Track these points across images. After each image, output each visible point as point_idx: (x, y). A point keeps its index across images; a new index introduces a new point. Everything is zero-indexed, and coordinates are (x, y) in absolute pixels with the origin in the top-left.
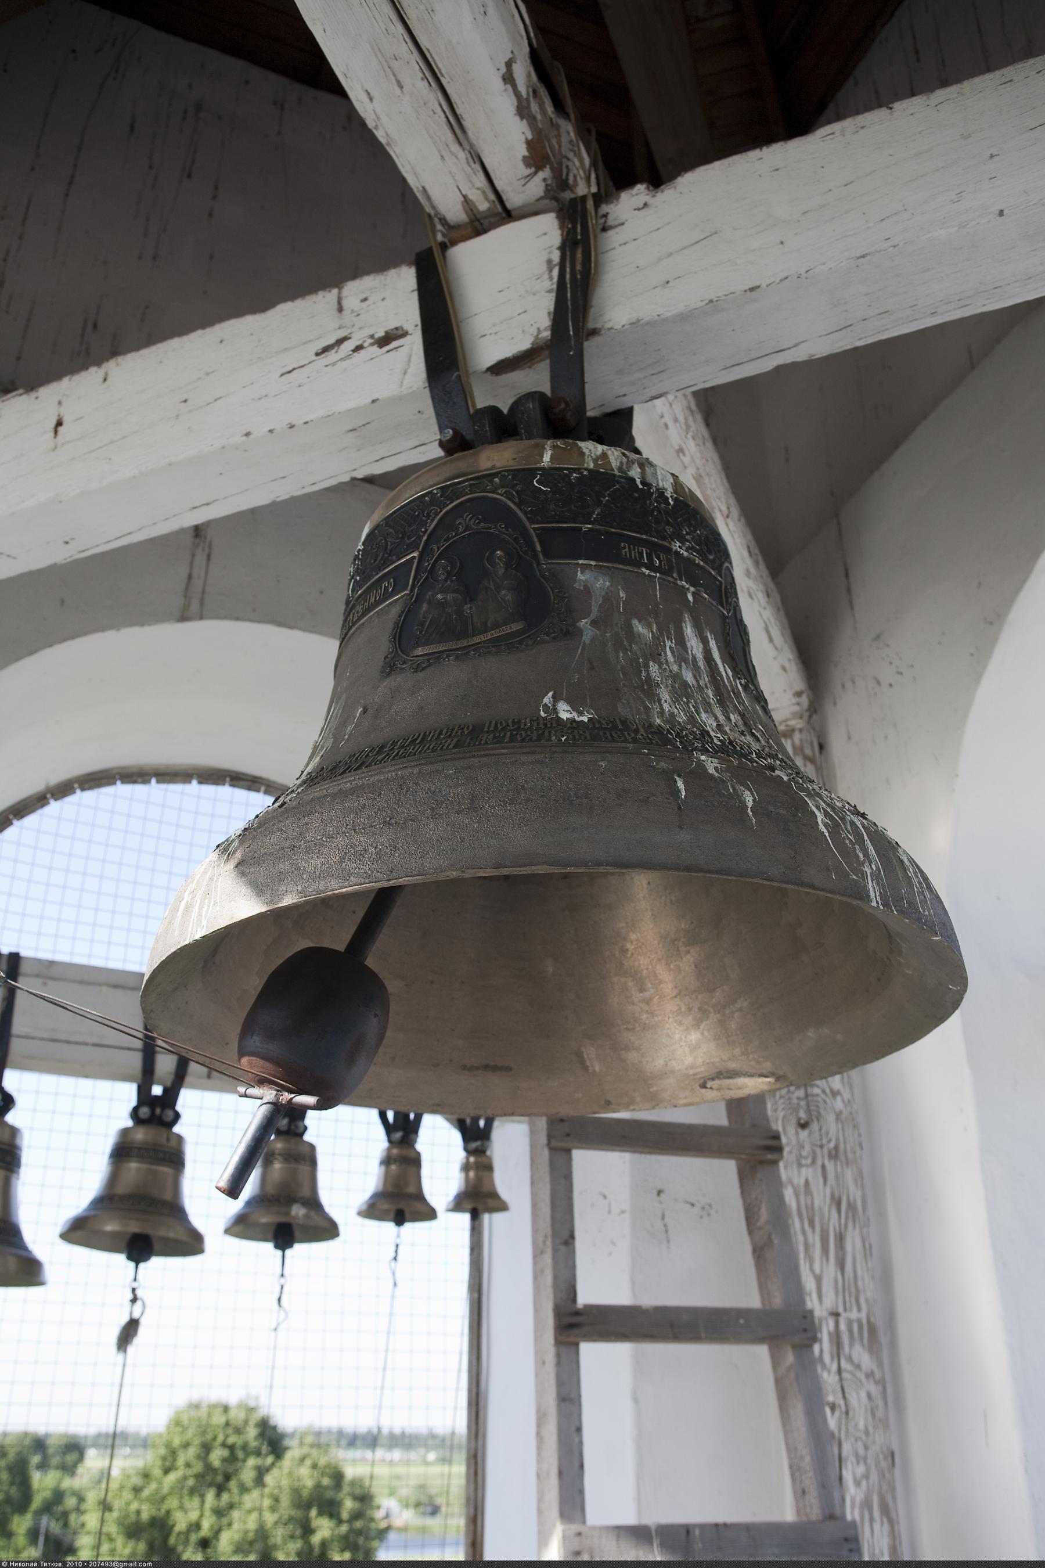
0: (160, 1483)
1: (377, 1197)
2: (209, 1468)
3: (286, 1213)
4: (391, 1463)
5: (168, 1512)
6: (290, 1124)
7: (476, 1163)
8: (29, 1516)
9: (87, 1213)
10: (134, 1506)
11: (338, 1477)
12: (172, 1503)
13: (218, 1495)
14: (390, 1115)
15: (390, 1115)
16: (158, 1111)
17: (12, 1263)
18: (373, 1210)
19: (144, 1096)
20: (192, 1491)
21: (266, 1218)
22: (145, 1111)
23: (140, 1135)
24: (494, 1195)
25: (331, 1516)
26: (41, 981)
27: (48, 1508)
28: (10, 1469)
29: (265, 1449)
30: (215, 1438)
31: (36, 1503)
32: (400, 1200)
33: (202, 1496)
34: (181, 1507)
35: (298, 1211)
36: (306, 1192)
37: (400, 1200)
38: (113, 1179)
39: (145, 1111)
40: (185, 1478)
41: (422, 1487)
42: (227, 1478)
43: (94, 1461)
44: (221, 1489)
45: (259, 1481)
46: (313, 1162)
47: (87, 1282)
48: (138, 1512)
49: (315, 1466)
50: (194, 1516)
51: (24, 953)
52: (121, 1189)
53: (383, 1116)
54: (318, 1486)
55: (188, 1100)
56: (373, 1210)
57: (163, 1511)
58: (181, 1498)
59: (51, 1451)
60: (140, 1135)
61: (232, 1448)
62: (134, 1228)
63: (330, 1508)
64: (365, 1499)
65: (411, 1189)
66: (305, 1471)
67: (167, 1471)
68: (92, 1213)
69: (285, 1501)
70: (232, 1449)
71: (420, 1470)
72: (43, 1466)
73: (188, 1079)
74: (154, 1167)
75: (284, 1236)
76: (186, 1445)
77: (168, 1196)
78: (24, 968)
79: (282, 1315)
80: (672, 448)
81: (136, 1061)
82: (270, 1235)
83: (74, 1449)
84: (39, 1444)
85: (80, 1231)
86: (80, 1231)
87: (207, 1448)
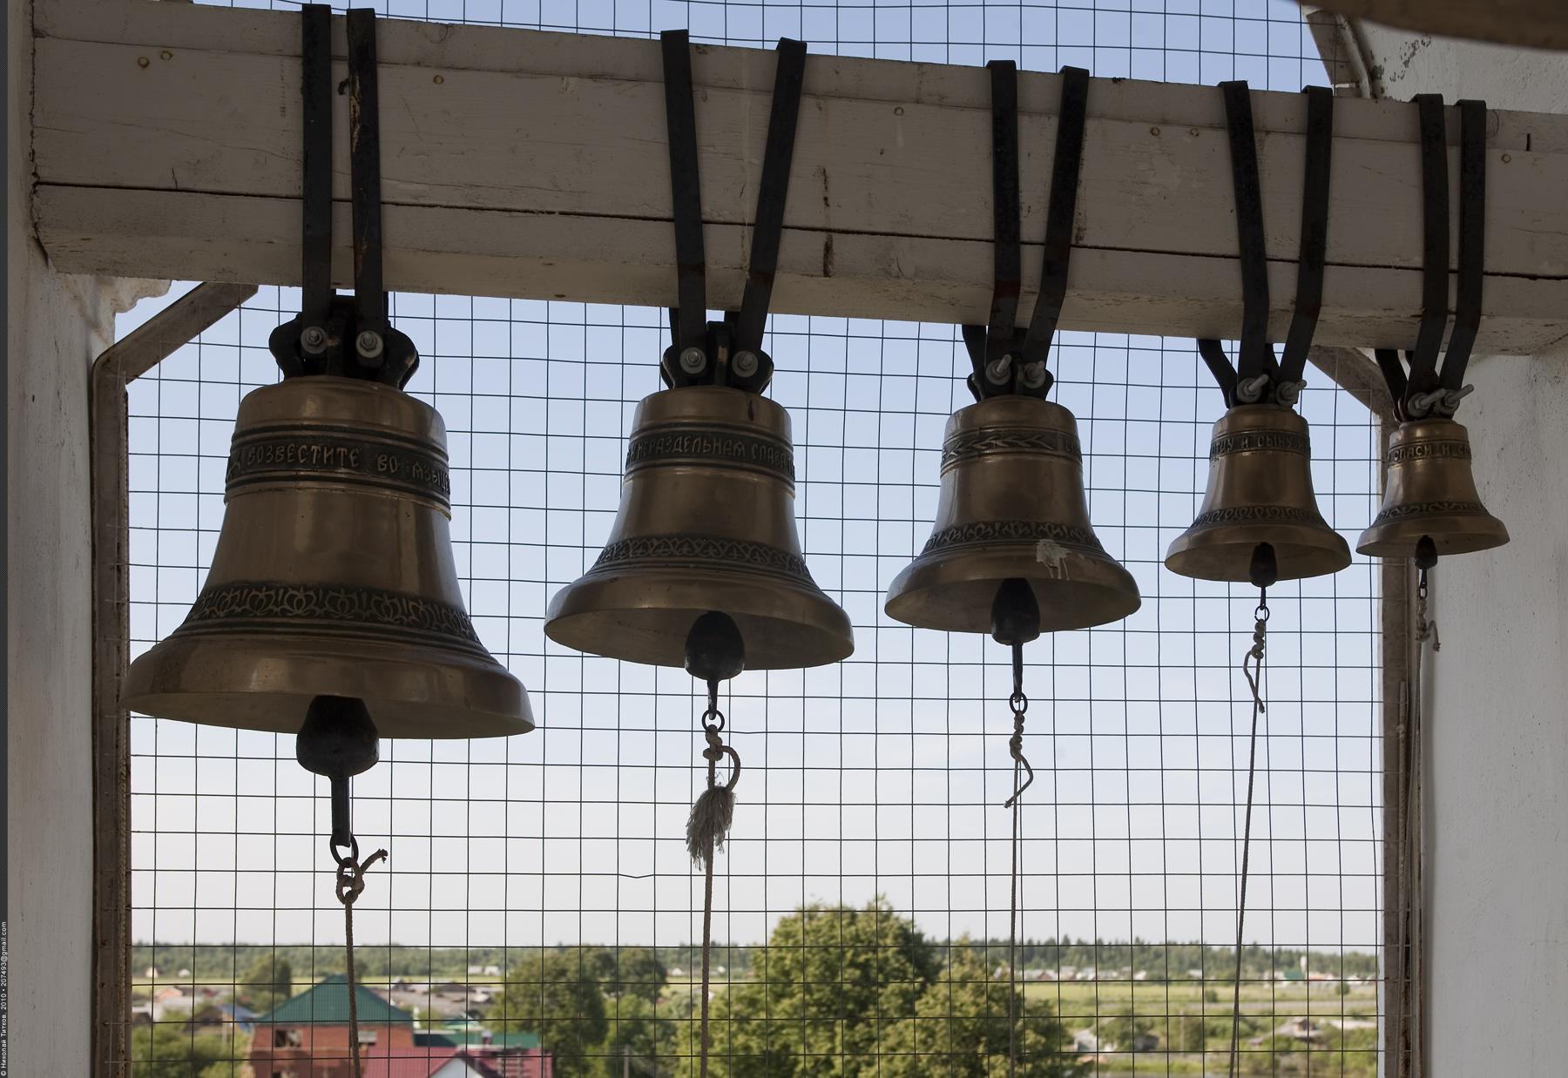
0: (768, 1011)
1: (1206, 523)
2: (838, 992)
3: (1017, 558)
4: (1084, 981)
5: (786, 1047)
6: (1012, 367)
7: (1429, 439)
8: (606, 1048)
9: (592, 579)
10: (741, 1039)
11: (1015, 1003)
12: (791, 1035)
13: (851, 1027)
14: (1231, 349)
15: (1231, 349)
16: (722, 354)
17: (455, 683)
18: (1201, 556)
19: (685, 326)
20: (816, 1023)
21: (977, 571)
22: (693, 358)
23: (691, 407)
24: (1475, 509)
25: (1006, 1052)
26: (430, 73)
27: (625, 1038)
28: (572, 988)
29: (910, 969)
30: (842, 955)
31: (612, 1032)
32: (1259, 529)
33: (830, 1027)
34: (803, 1040)
35: (1050, 553)
36: (1058, 513)
37: (1259, 529)
38: (640, 507)
39: (693, 358)
40: (805, 1005)
41: (1129, 1016)
42: (863, 1005)
43: (679, 986)
44: (853, 1020)
45: (908, 1010)
46: (1073, 453)
47: (619, 721)
48: (747, 1048)
49: (978, 991)
50: (822, 1048)
51: (380, 11)
52: (663, 523)
53: (1210, 351)
54: (985, 1016)
55: (784, 336)
56: (1201, 556)
57: (777, 1047)
58: (803, 1029)
59: (623, 970)
60: (691, 407)
61: (864, 967)
62: (700, 602)
63: (1003, 1042)
64: (1053, 1031)
65: (1290, 501)
66: (965, 996)
67: (779, 997)
68: (608, 575)
69: (941, 1028)
70: (859, 967)
71: (1125, 991)
72: (616, 987)
73: (782, 280)
74: (727, 474)
75: (1016, 613)
76: (802, 965)
77: (761, 533)
78: (388, 47)
79: (1025, 776)
80: (570, 1069)
81: (661, 243)
82: (987, 615)
83: (649, 968)
84: (607, 959)
85: (584, 619)
86: (584, 619)
87: (831, 969)
